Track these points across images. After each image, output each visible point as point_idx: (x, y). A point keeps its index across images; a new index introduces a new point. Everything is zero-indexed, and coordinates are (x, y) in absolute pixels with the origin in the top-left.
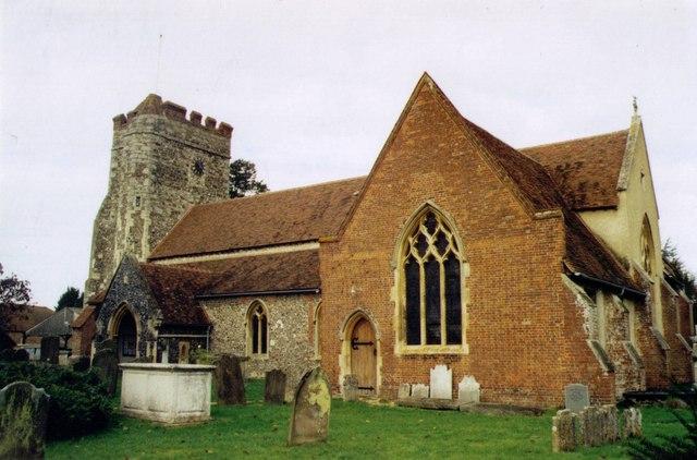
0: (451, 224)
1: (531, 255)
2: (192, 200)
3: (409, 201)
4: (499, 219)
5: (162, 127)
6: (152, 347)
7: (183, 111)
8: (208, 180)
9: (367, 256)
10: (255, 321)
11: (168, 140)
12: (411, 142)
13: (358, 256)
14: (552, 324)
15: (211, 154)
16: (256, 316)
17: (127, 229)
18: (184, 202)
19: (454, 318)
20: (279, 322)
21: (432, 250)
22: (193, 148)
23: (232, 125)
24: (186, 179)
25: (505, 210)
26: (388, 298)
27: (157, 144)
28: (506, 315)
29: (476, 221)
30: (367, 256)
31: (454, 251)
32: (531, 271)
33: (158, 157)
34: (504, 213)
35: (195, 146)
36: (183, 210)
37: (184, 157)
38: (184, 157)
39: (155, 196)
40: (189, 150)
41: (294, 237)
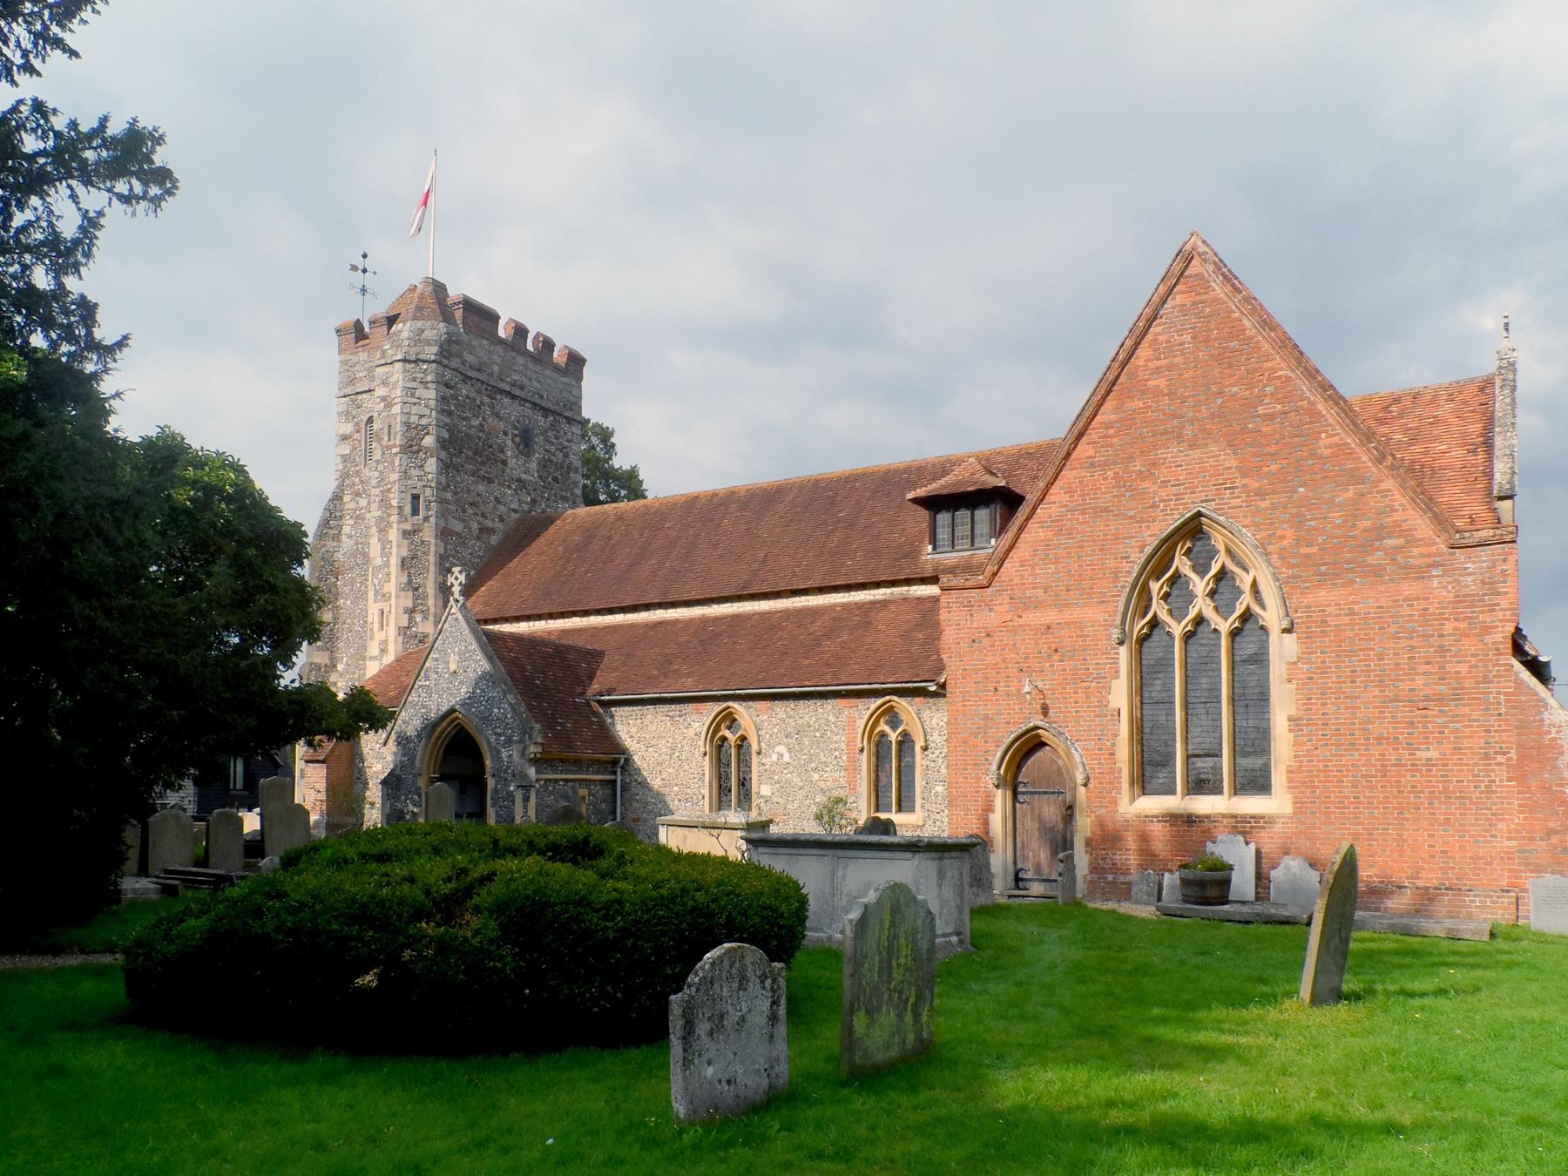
0: (1248, 552)
1: (1442, 619)
2: (514, 506)
3: (1154, 506)
4: (1366, 547)
5: (455, 348)
6: (526, 799)
7: (493, 318)
8: (544, 465)
9: (1052, 616)
10: (880, 748)
11: (466, 378)
12: (1159, 382)
13: (1032, 618)
14: (1487, 756)
15: (546, 411)
16: (883, 735)
17: (394, 561)
18: (502, 508)
19: (1253, 742)
20: (781, 749)
21: (1201, 605)
22: (514, 397)
23: (584, 355)
24: (504, 463)
25: (1382, 527)
26: (1103, 704)
27: (447, 385)
28: (1379, 739)
29: (1314, 550)
30: (1052, 616)
31: (1256, 609)
32: (1442, 650)
33: (450, 414)
34: (1380, 532)
35: (517, 392)
36: (499, 525)
37: (497, 415)
38: (497, 415)
39: (448, 496)
40: (506, 400)
41: (851, 569)
